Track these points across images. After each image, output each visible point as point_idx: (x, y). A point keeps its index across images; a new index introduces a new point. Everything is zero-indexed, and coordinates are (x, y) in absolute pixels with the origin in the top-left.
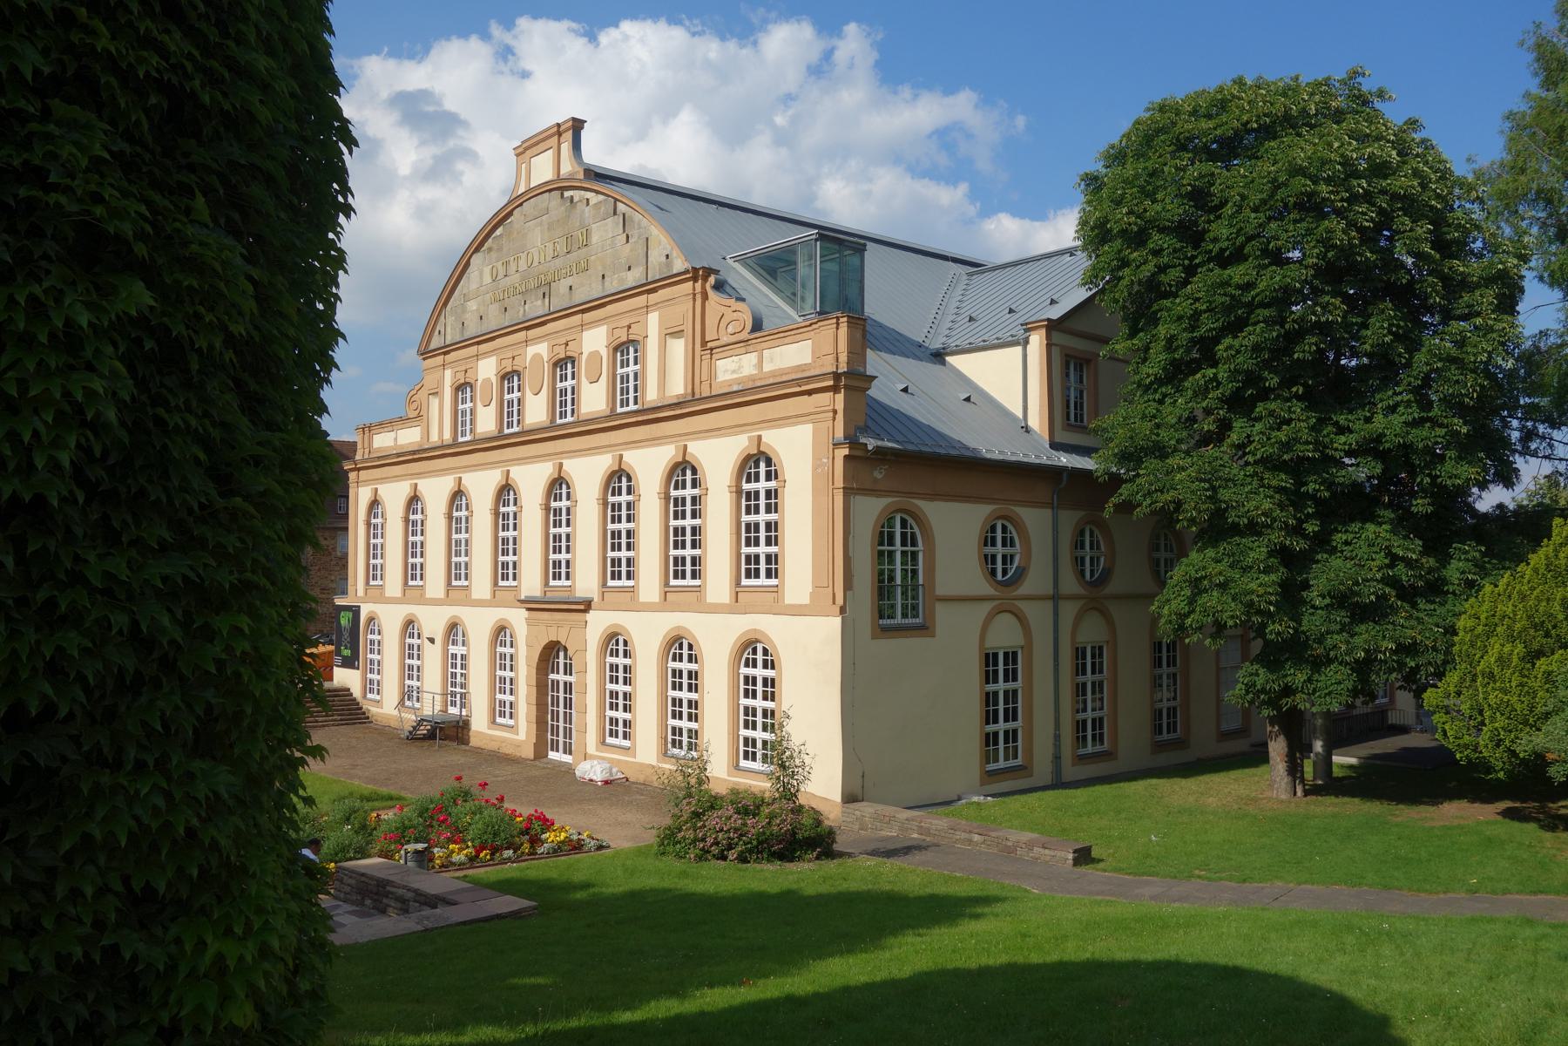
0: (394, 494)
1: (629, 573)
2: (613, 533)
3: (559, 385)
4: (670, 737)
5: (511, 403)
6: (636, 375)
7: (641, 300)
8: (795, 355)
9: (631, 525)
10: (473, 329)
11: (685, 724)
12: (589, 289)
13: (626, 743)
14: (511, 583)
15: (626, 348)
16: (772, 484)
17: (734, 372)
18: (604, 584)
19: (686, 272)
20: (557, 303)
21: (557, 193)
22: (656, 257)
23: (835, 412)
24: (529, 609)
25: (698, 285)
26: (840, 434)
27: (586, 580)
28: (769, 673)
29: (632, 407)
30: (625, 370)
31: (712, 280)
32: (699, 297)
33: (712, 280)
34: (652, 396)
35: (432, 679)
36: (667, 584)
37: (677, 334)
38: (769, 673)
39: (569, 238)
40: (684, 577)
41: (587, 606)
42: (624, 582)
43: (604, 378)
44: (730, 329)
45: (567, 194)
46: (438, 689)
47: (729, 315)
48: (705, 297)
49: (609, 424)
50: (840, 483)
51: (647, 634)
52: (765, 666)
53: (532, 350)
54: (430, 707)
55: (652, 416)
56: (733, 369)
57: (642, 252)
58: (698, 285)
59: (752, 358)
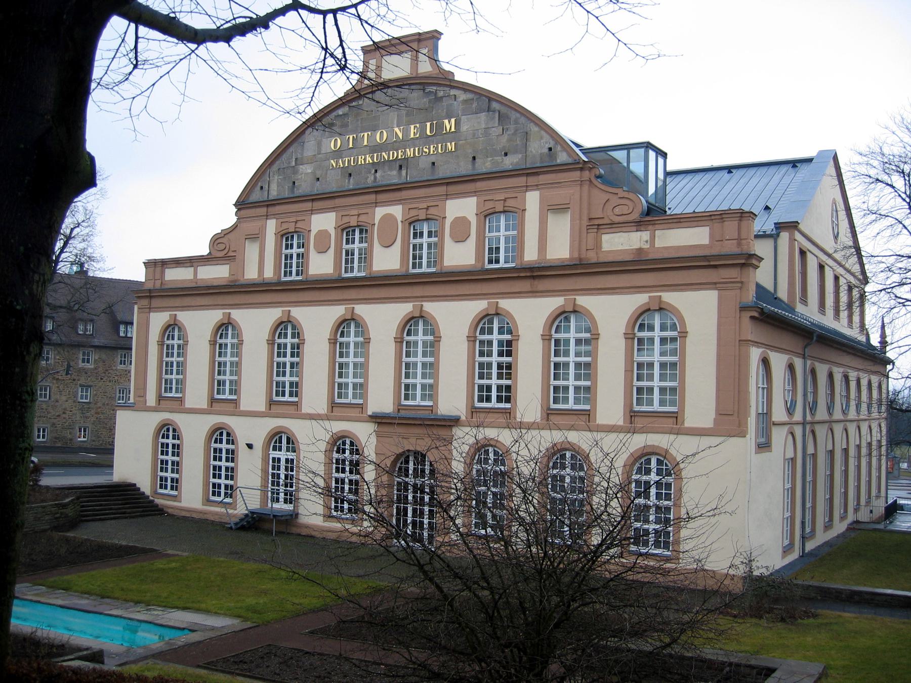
7: (521, 181)
10: (304, 187)
13: (174, 493)
24: (379, 423)
28: (176, 442)
34: (531, 255)
35: (250, 473)
38: (176, 442)
41: (453, 422)
43: (332, 251)
44: (617, 210)
46: (257, 482)
52: (174, 438)
53: (380, 212)
54: (250, 497)
59: (645, 235)
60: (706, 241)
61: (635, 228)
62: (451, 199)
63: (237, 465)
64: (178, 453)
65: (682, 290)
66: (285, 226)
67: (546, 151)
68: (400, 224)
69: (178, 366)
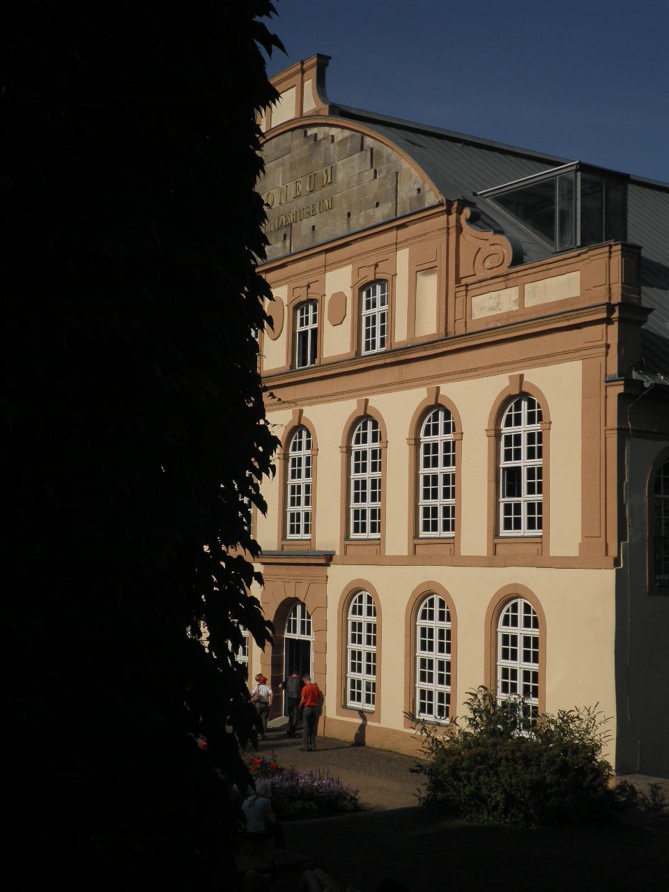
0: (329, 419)
1: (373, 525)
2: (357, 483)
3: (365, 312)
4: (349, 689)
5: (371, 320)
6: (383, 315)
7: (390, 237)
8: (560, 286)
9: (377, 475)
11: (435, 687)
12: (333, 227)
14: (440, 533)
15: (373, 286)
16: (536, 427)
17: (492, 309)
18: (347, 537)
19: (441, 204)
20: (298, 244)
21: (300, 131)
22: (406, 192)
23: (608, 346)
25: (453, 218)
26: (613, 369)
27: (328, 531)
29: (378, 349)
30: (372, 311)
31: (467, 212)
32: (453, 232)
33: (467, 212)
34: (400, 335)
36: (416, 536)
37: (429, 270)
39: (313, 178)
40: (435, 529)
41: (329, 558)
42: (368, 535)
44: (488, 264)
45: (311, 132)
47: (487, 249)
48: (459, 230)
49: (353, 367)
50: (613, 422)
51: (394, 588)
52: (442, 618)
55: (403, 357)
56: (489, 306)
57: (390, 186)
58: (453, 218)
59: (513, 292)
60: (576, 292)
61: (503, 285)
62: (331, 270)
63: (543, 667)
64: (536, 654)
65: (545, 364)
66: (363, 272)
67: (415, 193)
68: (286, 308)
69: (374, 486)
